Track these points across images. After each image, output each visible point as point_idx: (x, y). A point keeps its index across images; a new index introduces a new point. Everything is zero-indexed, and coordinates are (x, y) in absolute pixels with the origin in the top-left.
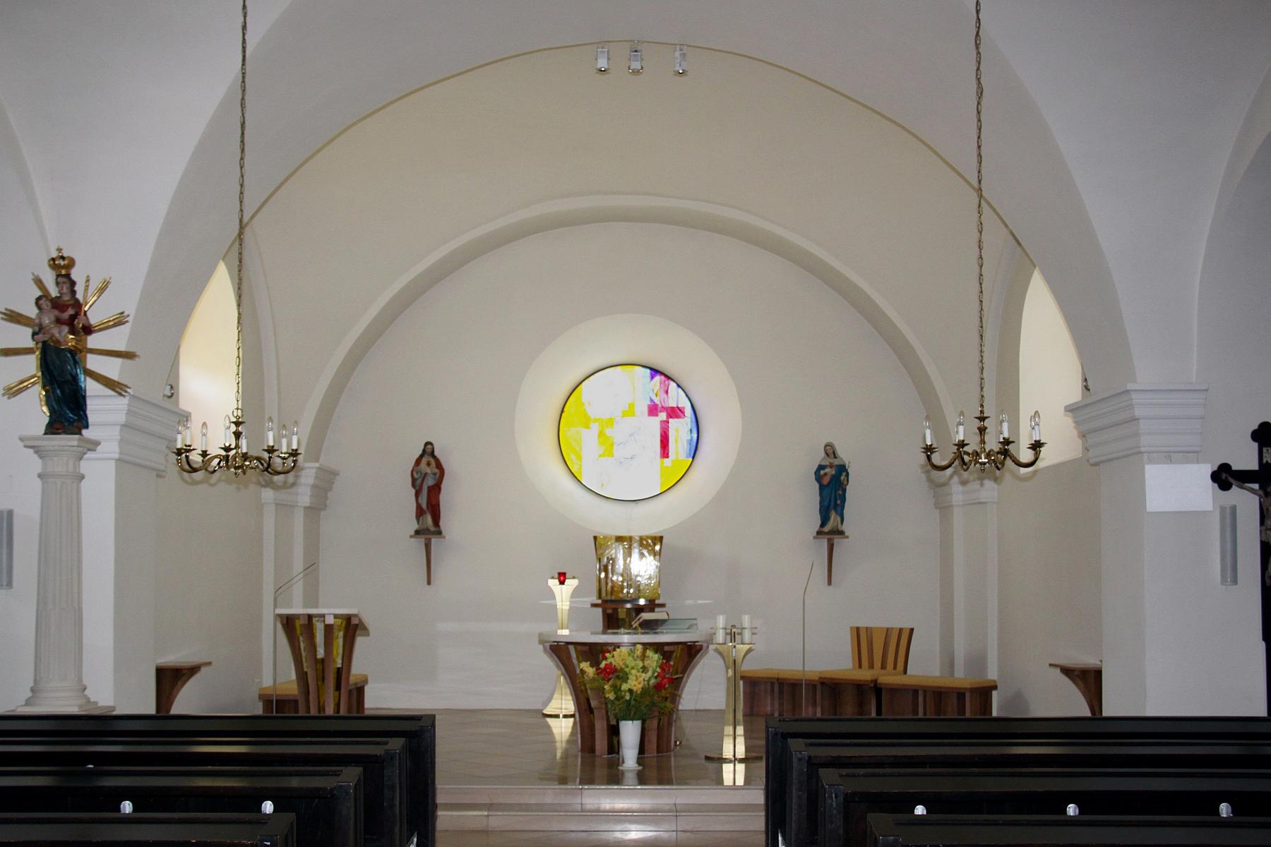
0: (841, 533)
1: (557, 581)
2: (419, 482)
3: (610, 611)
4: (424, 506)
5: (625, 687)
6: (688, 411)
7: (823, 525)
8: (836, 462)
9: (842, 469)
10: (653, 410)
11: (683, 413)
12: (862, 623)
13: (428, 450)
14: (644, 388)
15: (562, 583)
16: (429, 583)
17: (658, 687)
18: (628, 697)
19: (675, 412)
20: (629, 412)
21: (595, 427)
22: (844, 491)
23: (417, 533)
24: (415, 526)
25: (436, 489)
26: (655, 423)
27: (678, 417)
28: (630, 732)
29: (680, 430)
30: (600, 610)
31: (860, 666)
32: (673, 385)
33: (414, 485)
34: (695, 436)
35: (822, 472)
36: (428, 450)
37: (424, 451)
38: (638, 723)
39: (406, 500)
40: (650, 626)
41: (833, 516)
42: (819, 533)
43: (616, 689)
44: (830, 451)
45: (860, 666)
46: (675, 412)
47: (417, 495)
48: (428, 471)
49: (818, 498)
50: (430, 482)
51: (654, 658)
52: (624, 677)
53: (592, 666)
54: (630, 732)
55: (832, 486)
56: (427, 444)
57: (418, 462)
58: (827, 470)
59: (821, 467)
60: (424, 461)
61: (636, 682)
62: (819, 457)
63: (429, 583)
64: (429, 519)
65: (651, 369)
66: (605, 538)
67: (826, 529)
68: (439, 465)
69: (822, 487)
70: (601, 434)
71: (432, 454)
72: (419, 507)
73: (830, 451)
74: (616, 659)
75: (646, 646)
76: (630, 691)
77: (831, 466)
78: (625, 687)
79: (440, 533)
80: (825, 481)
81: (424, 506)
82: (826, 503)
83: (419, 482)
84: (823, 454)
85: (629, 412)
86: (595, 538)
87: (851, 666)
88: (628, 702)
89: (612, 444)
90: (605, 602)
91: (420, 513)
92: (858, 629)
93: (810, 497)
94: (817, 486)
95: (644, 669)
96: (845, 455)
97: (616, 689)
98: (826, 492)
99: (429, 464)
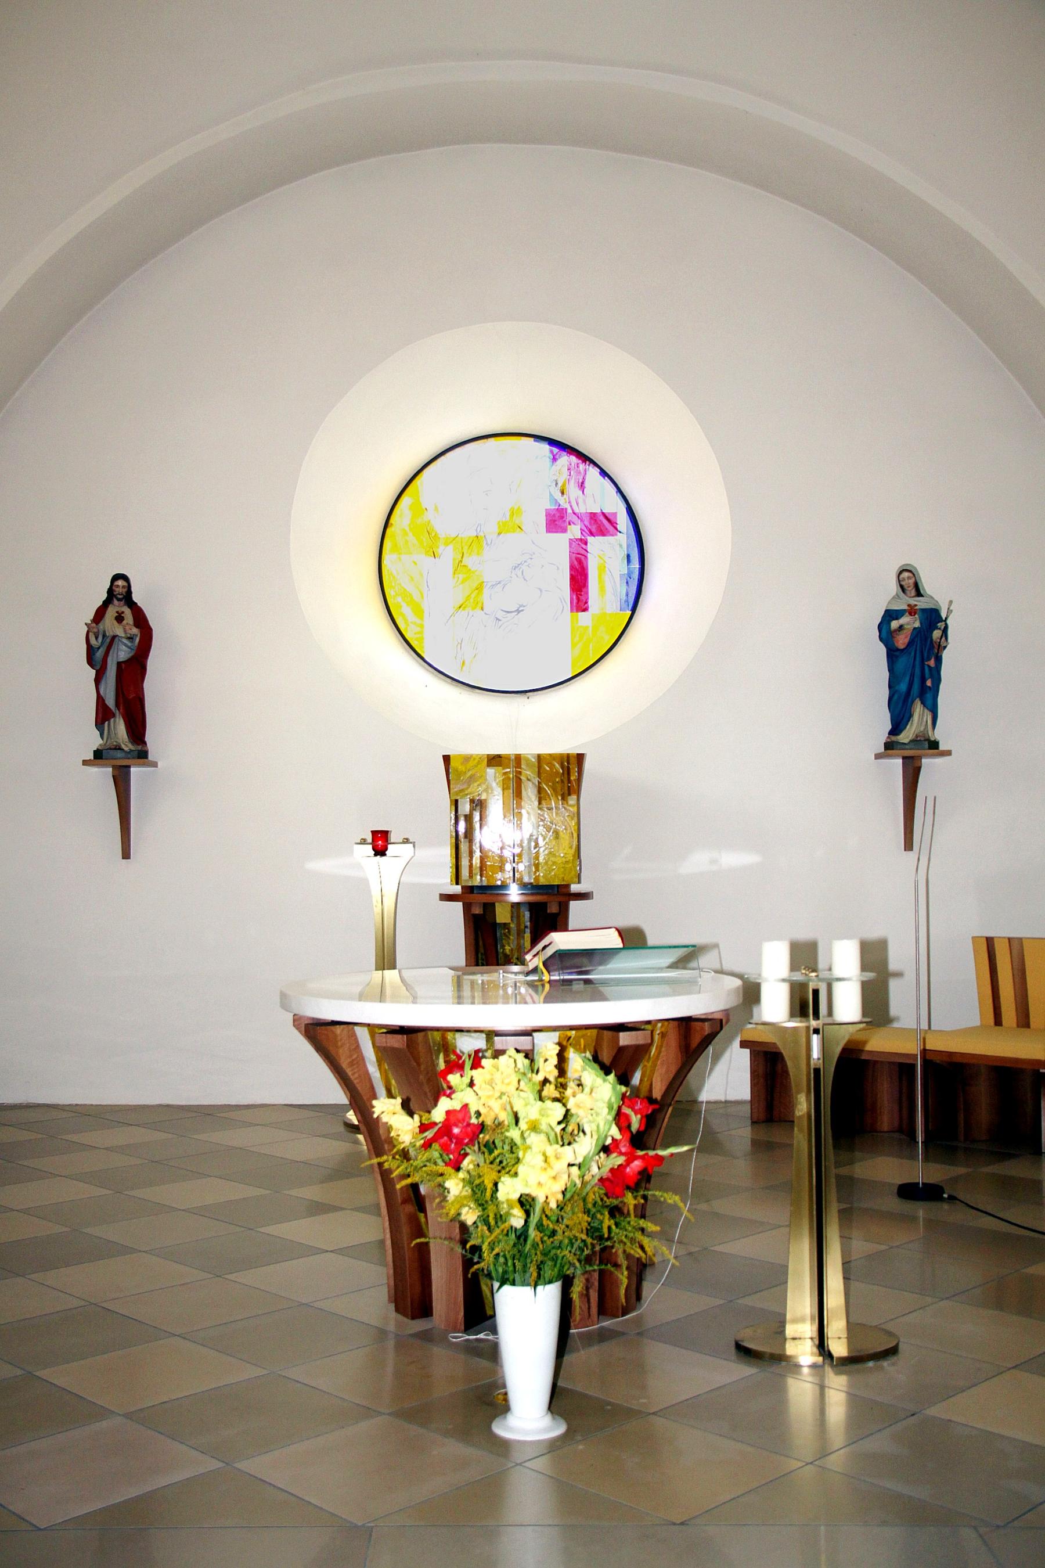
0: (934, 745)
1: (369, 849)
2: (99, 654)
3: (477, 910)
4: (110, 702)
5: (509, 1190)
6: (623, 521)
7: (897, 728)
8: (921, 603)
9: (932, 618)
10: (556, 521)
11: (613, 524)
12: (1001, 930)
13: (119, 592)
14: (542, 477)
15: (380, 852)
16: (126, 855)
17: (613, 1183)
18: (517, 1220)
19: (600, 524)
20: (511, 524)
21: (448, 555)
22: (939, 660)
23: (98, 754)
24: (95, 741)
25: (133, 672)
26: (558, 549)
27: (602, 532)
28: (526, 1320)
29: (607, 556)
30: (458, 906)
31: (998, 1021)
32: (593, 472)
33: (90, 661)
34: (636, 565)
35: (894, 624)
36: (119, 592)
37: (110, 591)
38: (550, 1294)
39: (79, 688)
40: (575, 972)
41: (919, 713)
42: (889, 746)
43: (483, 1195)
44: (909, 582)
45: (998, 1021)
46: (600, 524)
47: (98, 681)
48: (119, 631)
49: (886, 674)
50: (123, 652)
51: (597, 1096)
52: (506, 1160)
53: (407, 1107)
54: (526, 1320)
55: (914, 652)
56: (116, 577)
57: (100, 614)
58: (905, 620)
59: (890, 615)
60: (111, 612)
61: (544, 1174)
62: (887, 593)
63: (126, 855)
64: (120, 728)
65: (552, 442)
66: (467, 759)
67: (905, 737)
68: (141, 620)
69: (893, 654)
70: (459, 565)
71: (128, 598)
72: (100, 701)
73: (909, 582)
74: (487, 1092)
75: (569, 1038)
76: (526, 1203)
77: (912, 611)
78: (509, 1190)
79: (142, 755)
80: (902, 641)
81: (110, 702)
82: (903, 687)
83: (99, 654)
84: (893, 588)
85: (511, 524)
86: (447, 759)
87: (975, 1021)
88: (522, 1235)
89: (479, 588)
90: (469, 890)
91: (103, 715)
92: (990, 941)
93: (865, 679)
94: (882, 650)
95: (568, 1132)
96: (938, 589)
97: (483, 1195)
98: (902, 662)
99: (119, 619)
